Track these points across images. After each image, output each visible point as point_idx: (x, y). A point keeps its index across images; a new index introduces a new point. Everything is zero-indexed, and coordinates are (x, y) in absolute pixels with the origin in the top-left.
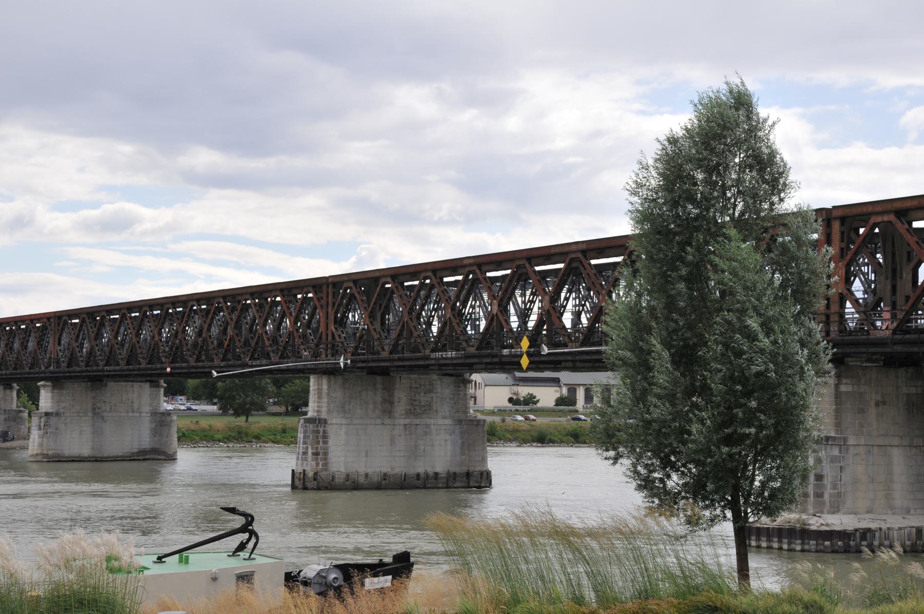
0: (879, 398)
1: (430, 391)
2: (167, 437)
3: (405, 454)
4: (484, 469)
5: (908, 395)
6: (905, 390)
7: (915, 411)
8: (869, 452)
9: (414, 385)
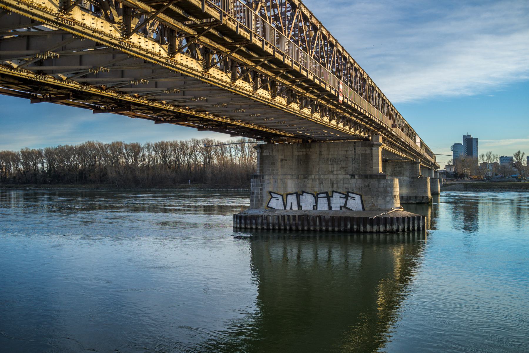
0: (283, 157)
1: (401, 167)
2: (434, 186)
3: (97, 176)
4: (426, 195)
5: (298, 156)
6: (296, 153)
7: (302, 163)
8: (275, 182)
9: (394, 165)
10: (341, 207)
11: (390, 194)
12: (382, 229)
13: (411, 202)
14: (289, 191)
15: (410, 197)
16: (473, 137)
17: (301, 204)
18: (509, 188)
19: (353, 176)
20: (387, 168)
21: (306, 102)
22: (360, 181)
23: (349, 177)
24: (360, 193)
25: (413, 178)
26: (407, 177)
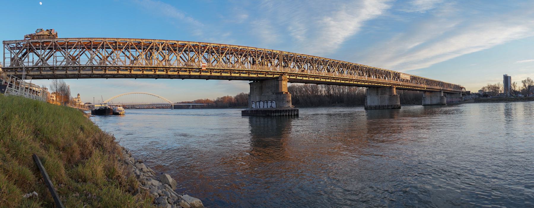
10: (270, 106)
11: (285, 101)
12: (277, 115)
13: (389, 108)
14: (257, 101)
15: (389, 105)
16: (509, 75)
17: (260, 106)
18: (497, 101)
19: (273, 93)
20: (379, 91)
21: (29, 71)
22: (275, 95)
23: (272, 94)
24: (275, 100)
25: (390, 95)
26: (388, 95)
